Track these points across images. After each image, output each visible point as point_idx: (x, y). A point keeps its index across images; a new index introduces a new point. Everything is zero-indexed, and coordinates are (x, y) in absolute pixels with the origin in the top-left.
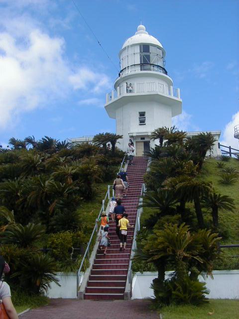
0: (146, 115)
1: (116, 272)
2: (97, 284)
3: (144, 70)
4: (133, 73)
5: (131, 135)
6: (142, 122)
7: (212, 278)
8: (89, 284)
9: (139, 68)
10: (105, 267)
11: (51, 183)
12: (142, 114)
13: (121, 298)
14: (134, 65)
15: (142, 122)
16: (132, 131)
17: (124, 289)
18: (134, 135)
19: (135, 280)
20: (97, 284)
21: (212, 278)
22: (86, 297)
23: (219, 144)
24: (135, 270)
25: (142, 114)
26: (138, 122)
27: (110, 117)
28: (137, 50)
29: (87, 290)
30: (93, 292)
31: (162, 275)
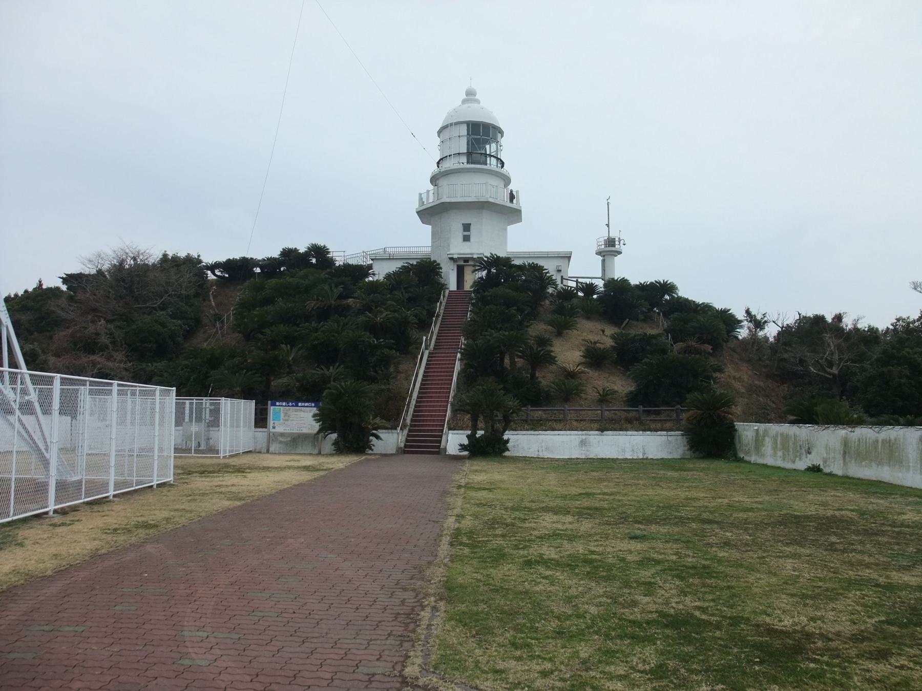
0: (472, 228)
1: (431, 431)
2: (414, 436)
3: (472, 163)
4: (457, 166)
5: (451, 256)
6: (466, 239)
7: (581, 356)
8: (407, 441)
9: (464, 159)
10: (422, 426)
11: (373, 380)
12: (467, 227)
13: (438, 453)
14: (459, 154)
15: (466, 239)
16: (452, 251)
17: (440, 446)
18: (455, 256)
19: (450, 435)
20: (414, 436)
21: (581, 356)
22: (405, 452)
23: (562, 277)
24: (450, 429)
25: (467, 227)
26: (461, 239)
27: (423, 223)
28: (463, 130)
29: (406, 446)
30: (411, 448)
31: (474, 433)
